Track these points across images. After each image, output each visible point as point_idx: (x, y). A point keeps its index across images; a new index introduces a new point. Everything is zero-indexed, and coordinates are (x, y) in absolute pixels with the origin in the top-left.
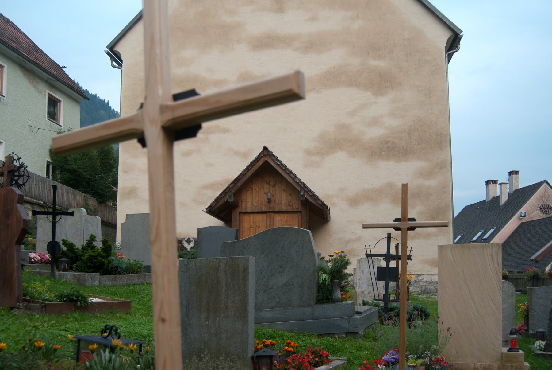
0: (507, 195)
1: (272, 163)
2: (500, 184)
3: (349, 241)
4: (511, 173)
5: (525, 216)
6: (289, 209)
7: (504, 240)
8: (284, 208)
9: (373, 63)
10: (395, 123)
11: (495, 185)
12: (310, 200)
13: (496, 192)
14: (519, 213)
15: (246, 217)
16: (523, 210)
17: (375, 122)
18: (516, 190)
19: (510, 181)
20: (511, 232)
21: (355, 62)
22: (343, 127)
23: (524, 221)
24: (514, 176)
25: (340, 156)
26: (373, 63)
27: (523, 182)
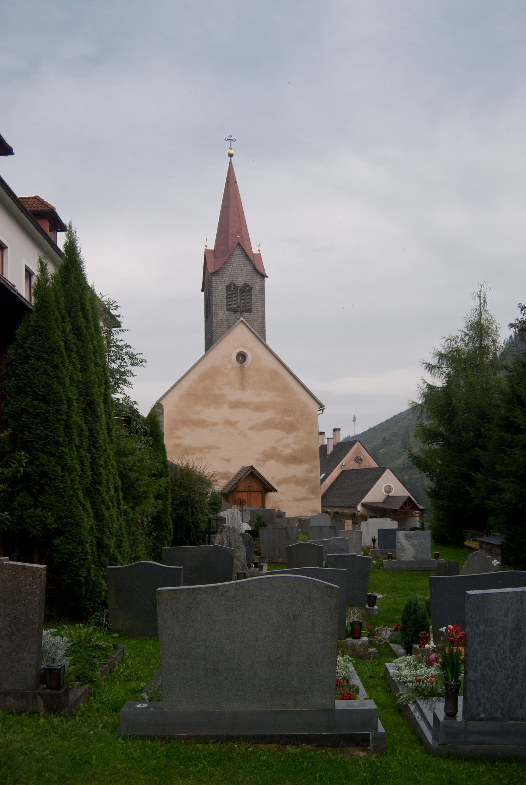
0: (332, 447)
1: (254, 472)
2: (328, 438)
3: (277, 502)
4: (335, 430)
5: (345, 466)
6: (258, 490)
7: (332, 482)
8: (255, 490)
9: (286, 418)
10: (296, 447)
11: (323, 435)
12: (270, 488)
13: (324, 442)
14: (341, 463)
15: (238, 494)
16: (343, 462)
17: (287, 446)
18: (338, 443)
19: (334, 435)
20: (336, 477)
21: (278, 417)
22: (273, 448)
23: (344, 469)
24: (337, 432)
25: (272, 462)
26: (286, 418)
27: (343, 436)
